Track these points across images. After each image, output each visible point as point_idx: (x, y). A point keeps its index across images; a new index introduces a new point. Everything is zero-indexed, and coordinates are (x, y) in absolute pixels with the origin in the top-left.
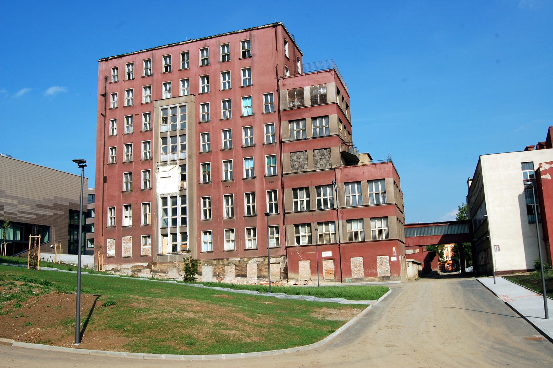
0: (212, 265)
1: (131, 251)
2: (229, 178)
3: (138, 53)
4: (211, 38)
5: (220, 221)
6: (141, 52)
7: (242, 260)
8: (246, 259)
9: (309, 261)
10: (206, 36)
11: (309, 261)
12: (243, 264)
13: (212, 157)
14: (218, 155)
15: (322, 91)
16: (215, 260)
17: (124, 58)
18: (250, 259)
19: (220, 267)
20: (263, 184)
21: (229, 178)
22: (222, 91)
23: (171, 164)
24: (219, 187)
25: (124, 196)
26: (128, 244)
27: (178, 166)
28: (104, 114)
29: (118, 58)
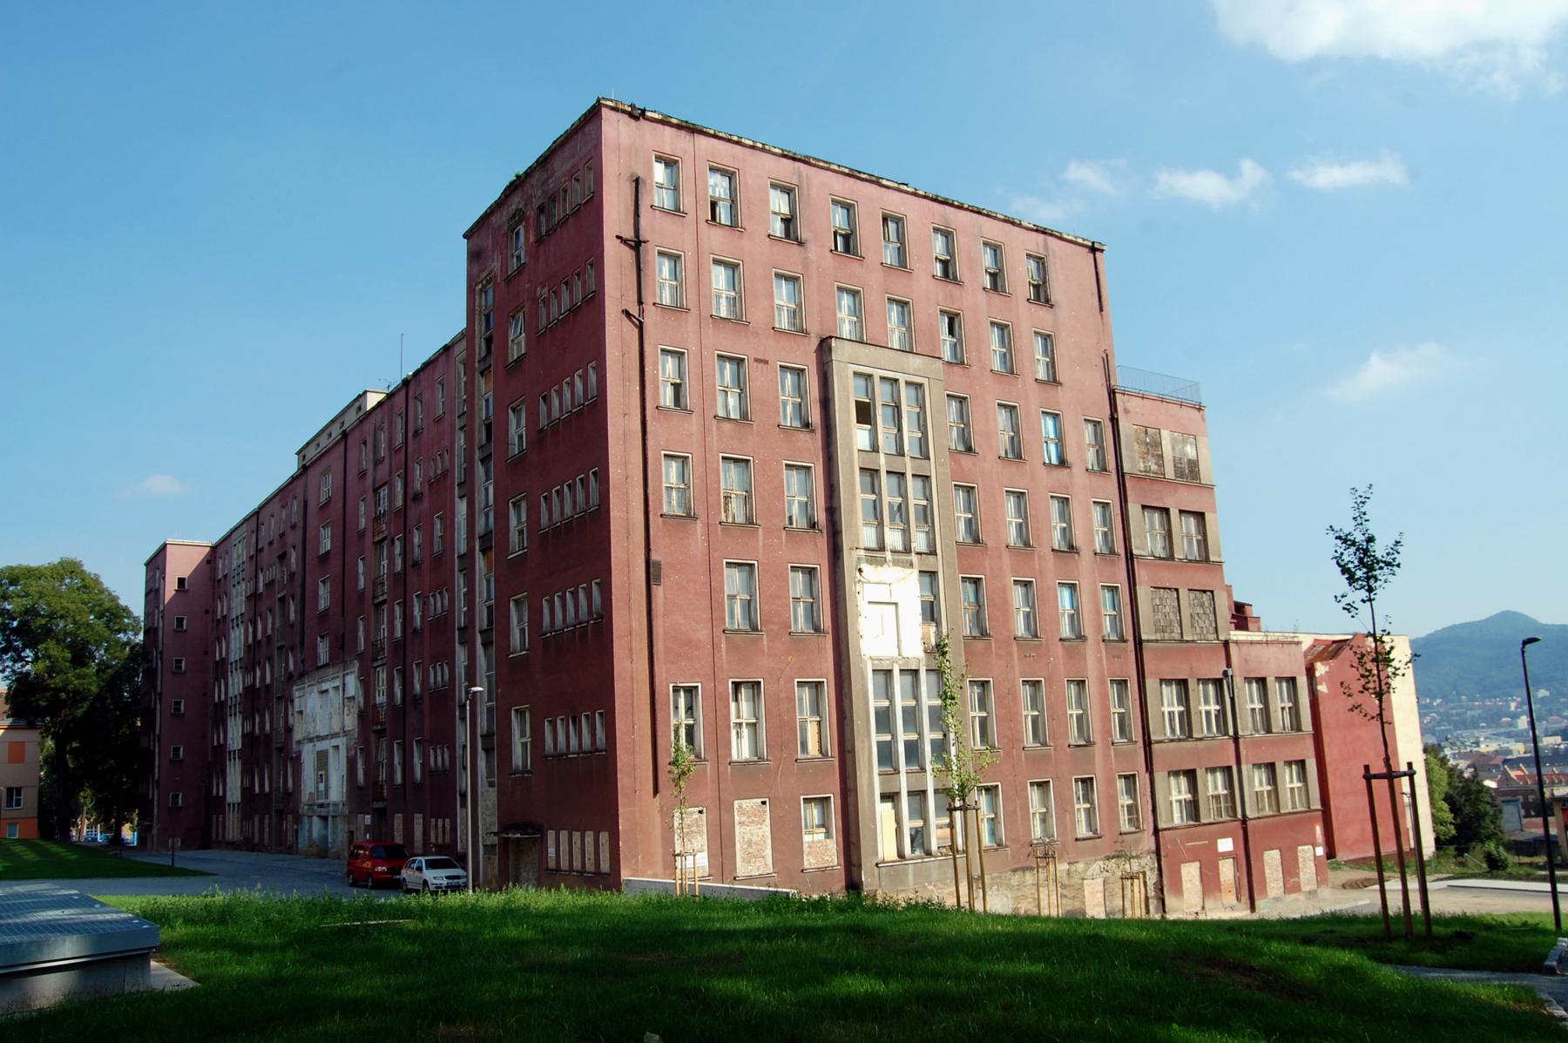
0: (1010, 887)
1: (768, 852)
2: (267, 789)
3: (753, 147)
4: (960, 207)
5: (1019, 755)
6: (763, 150)
7: (1073, 868)
8: (1081, 866)
9: (1197, 864)
10: (950, 196)
11: (1197, 864)
12: (1076, 880)
13: (987, 562)
14: (1000, 558)
15: (1190, 451)
16: (1014, 871)
17: (702, 140)
18: (1088, 865)
19: (1028, 893)
20: (1101, 659)
21: (267, 789)
22: (781, 332)
23: (896, 563)
24: (1011, 654)
25: (732, 647)
26: (754, 829)
27: (916, 572)
28: (634, 311)
29: (679, 127)
